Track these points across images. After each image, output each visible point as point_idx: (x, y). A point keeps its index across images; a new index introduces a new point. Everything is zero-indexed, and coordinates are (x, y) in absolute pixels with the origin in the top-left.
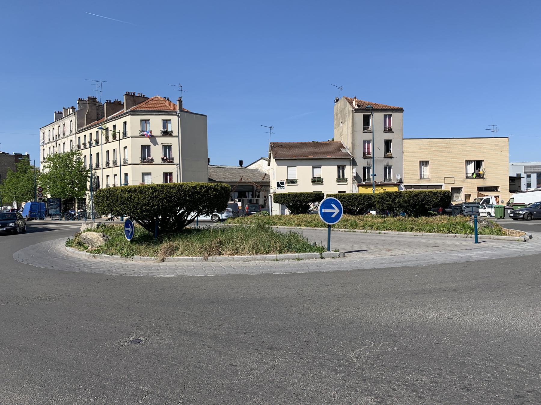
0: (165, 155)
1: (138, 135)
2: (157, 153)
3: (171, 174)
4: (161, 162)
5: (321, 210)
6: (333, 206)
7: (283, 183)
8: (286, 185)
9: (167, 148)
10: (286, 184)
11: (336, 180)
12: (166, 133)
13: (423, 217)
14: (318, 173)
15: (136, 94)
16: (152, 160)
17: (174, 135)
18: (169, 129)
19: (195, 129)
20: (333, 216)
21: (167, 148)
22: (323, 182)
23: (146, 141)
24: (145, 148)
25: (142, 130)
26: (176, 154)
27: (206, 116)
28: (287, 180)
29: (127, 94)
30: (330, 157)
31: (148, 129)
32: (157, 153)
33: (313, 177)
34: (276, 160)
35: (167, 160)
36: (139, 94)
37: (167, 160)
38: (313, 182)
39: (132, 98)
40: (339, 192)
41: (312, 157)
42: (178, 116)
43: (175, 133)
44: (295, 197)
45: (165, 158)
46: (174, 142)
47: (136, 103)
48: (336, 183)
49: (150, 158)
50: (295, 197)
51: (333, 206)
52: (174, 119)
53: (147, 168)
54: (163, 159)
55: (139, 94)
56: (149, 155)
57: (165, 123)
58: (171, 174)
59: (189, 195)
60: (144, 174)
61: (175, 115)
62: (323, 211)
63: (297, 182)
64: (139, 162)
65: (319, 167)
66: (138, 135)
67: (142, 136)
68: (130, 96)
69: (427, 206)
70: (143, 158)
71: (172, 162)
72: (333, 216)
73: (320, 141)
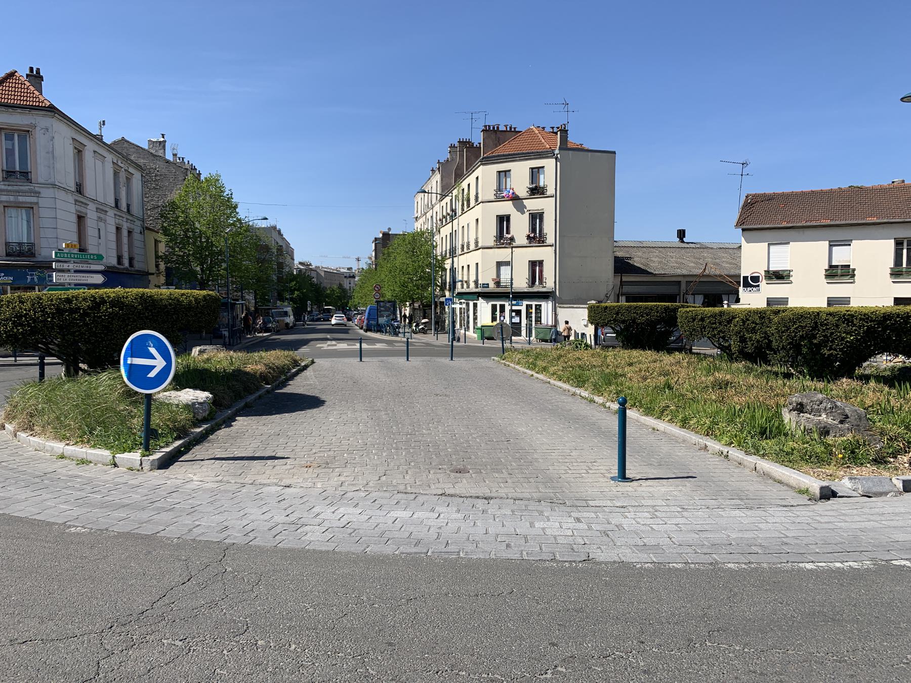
0: (533, 230)
1: (493, 198)
2: (520, 227)
3: (541, 263)
4: (525, 242)
5: (125, 360)
6: (153, 351)
7: (756, 279)
8: (763, 283)
9: (536, 218)
10: (764, 282)
11: (889, 271)
12: (537, 191)
13: (844, 380)
14: (841, 256)
15: (502, 128)
16: (512, 239)
17: (548, 193)
18: (542, 184)
19: (589, 177)
20: (152, 374)
21: (536, 218)
22: (853, 276)
23: (507, 208)
24: (503, 221)
25: (499, 189)
26: (549, 227)
27: (614, 153)
28: (767, 272)
29: (486, 130)
30: (875, 220)
31: (508, 187)
32: (520, 227)
33: (831, 266)
34: (743, 230)
35: (536, 238)
36: (506, 126)
37: (536, 238)
38: (827, 276)
39: (493, 136)
40: (898, 301)
41: (828, 222)
42: (556, 159)
43: (551, 191)
44: (617, 314)
45: (532, 235)
46: (547, 206)
47: (498, 144)
48: (889, 280)
49: (509, 236)
50: (617, 314)
51: (153, 351)
52: (549, 165)
53: (504, 254)
54: (528, 237)
55: (506, 126)
56: (508, 232)
57: (535, 173)
58: (541, 263)
59: (53, 314)
60: (499, 264)
61: (551, 157)
62: (129, 362)
63: (789, 276)
64: (492, 244)
65: (847, 243)
66: (493, 198)
67: (499, 198)
68: (494, 135)
69: (826, 352)
70: (500, 236)
71: (543, 242)
72: (152, 374)
73: (868, 182)
